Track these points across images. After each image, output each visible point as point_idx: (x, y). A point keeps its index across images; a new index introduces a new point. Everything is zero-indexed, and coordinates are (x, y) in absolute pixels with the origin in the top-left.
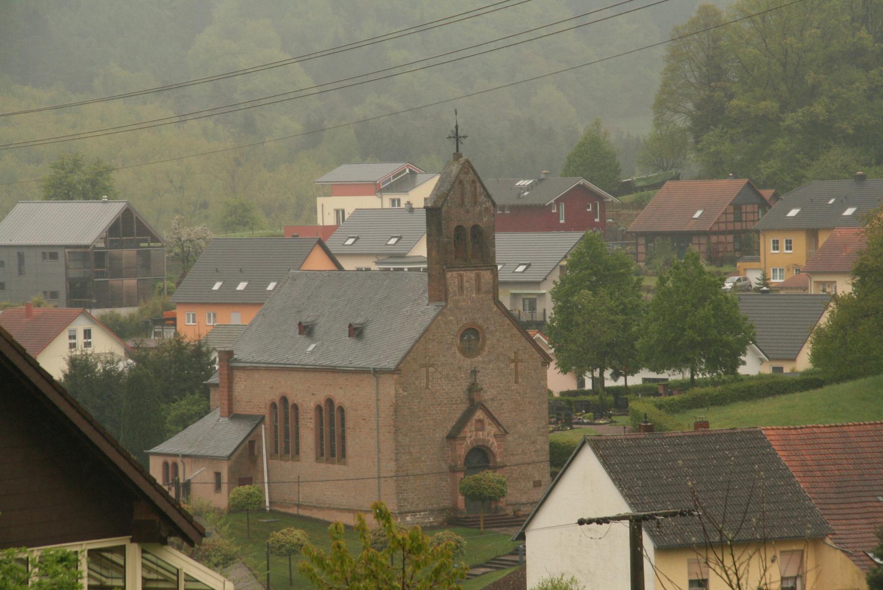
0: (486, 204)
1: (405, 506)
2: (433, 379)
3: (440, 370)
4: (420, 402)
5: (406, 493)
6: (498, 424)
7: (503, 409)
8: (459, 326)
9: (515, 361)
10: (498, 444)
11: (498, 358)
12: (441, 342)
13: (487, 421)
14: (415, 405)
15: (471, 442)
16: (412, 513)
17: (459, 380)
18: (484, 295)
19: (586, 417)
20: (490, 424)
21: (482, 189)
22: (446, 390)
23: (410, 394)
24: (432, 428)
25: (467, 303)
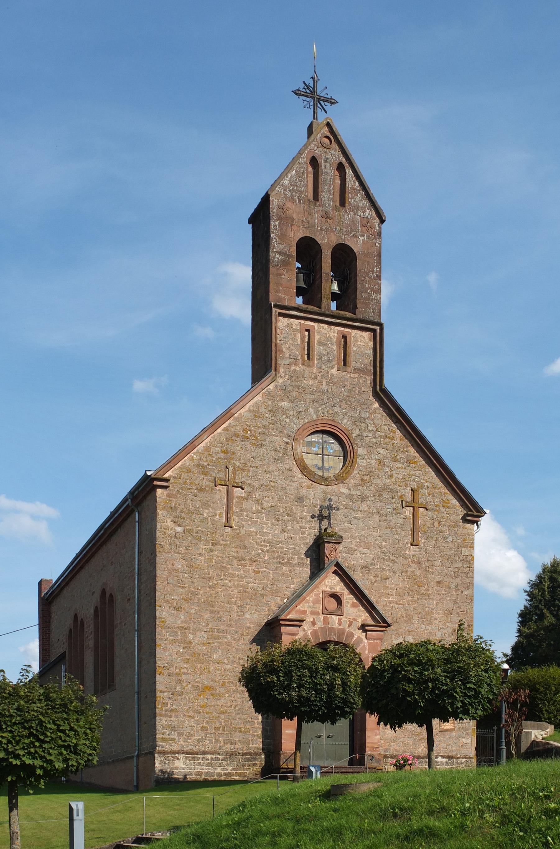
0: (364, 212)
1: (172, 740)
2: (242, 510)
3: (257, 495)
4: (211, 550)
5: (176, 717)
6: (370, 607)
7: (387, 588)
8: (301, 422)
9: (414, 505)
10: (369, 644)
11: (380, 495)
12: (262, 445)
13: (348, 598)
14: (201, 555)
15: (315, 633)
16: (187, 753)
17: (298, 522)
18: (356, 375)
19: (388, 756)
20: (353, 605)
21: (357, 184)
22: (270, 536)
23: (190, 531)
24: (235, 603)
25: (320, 382)
